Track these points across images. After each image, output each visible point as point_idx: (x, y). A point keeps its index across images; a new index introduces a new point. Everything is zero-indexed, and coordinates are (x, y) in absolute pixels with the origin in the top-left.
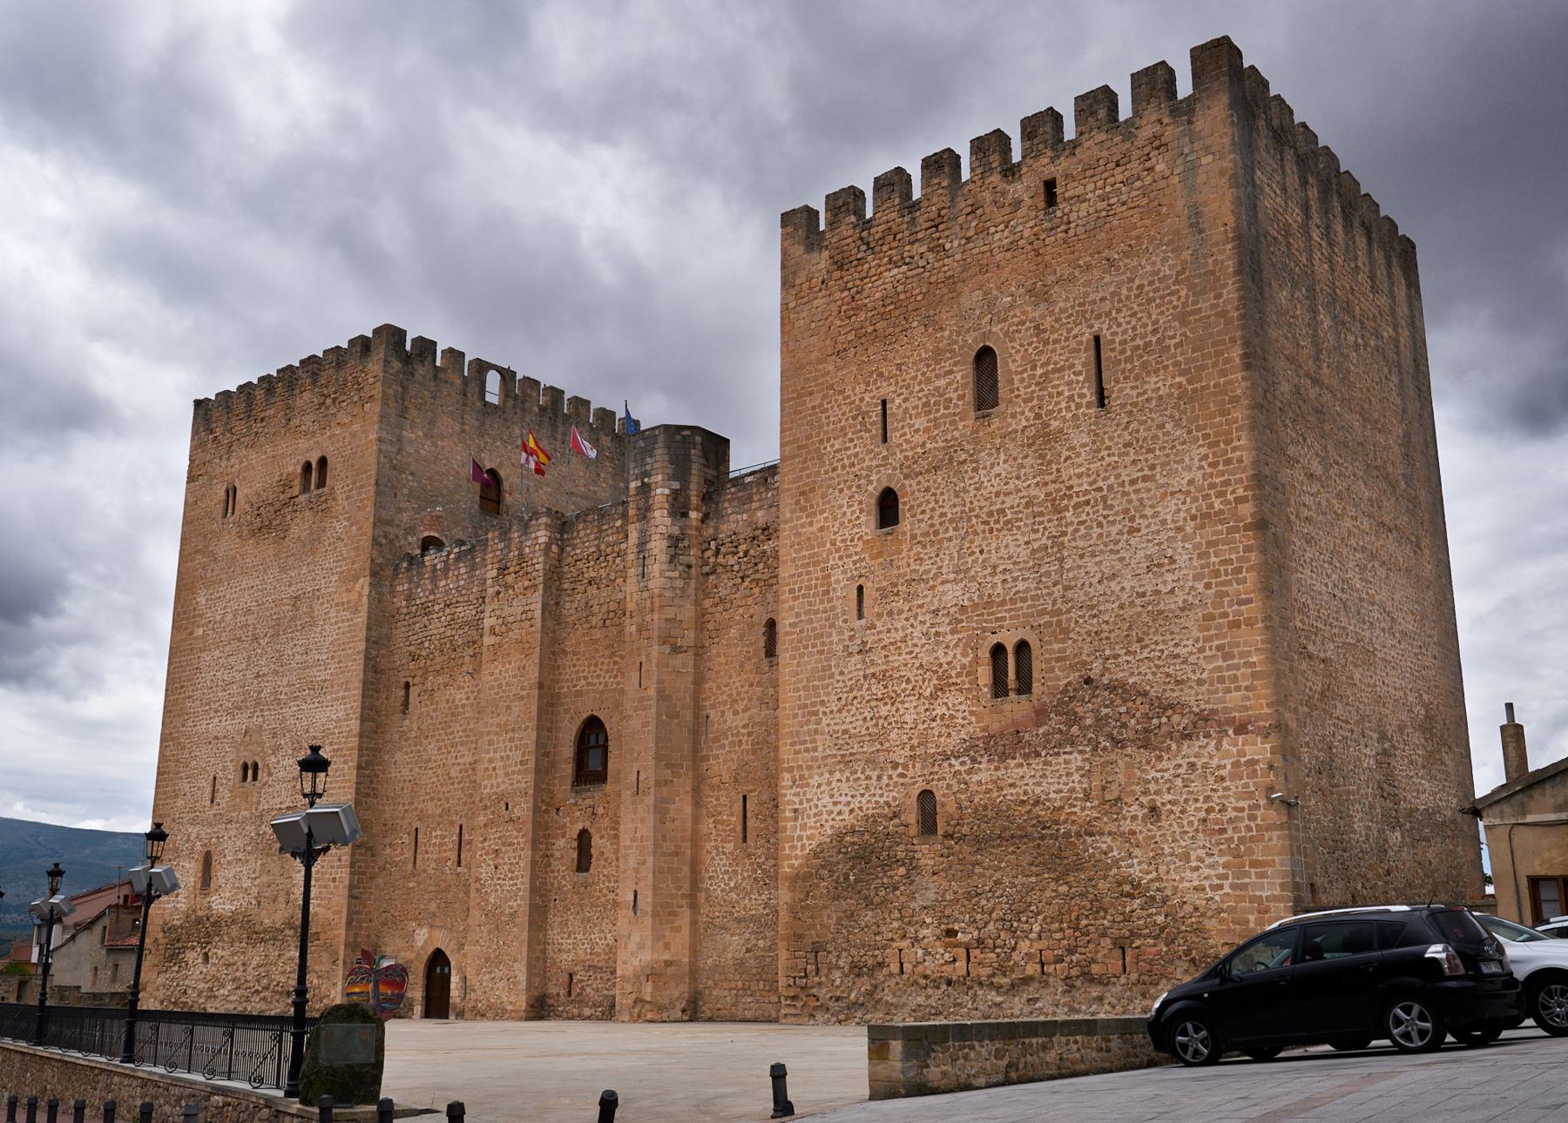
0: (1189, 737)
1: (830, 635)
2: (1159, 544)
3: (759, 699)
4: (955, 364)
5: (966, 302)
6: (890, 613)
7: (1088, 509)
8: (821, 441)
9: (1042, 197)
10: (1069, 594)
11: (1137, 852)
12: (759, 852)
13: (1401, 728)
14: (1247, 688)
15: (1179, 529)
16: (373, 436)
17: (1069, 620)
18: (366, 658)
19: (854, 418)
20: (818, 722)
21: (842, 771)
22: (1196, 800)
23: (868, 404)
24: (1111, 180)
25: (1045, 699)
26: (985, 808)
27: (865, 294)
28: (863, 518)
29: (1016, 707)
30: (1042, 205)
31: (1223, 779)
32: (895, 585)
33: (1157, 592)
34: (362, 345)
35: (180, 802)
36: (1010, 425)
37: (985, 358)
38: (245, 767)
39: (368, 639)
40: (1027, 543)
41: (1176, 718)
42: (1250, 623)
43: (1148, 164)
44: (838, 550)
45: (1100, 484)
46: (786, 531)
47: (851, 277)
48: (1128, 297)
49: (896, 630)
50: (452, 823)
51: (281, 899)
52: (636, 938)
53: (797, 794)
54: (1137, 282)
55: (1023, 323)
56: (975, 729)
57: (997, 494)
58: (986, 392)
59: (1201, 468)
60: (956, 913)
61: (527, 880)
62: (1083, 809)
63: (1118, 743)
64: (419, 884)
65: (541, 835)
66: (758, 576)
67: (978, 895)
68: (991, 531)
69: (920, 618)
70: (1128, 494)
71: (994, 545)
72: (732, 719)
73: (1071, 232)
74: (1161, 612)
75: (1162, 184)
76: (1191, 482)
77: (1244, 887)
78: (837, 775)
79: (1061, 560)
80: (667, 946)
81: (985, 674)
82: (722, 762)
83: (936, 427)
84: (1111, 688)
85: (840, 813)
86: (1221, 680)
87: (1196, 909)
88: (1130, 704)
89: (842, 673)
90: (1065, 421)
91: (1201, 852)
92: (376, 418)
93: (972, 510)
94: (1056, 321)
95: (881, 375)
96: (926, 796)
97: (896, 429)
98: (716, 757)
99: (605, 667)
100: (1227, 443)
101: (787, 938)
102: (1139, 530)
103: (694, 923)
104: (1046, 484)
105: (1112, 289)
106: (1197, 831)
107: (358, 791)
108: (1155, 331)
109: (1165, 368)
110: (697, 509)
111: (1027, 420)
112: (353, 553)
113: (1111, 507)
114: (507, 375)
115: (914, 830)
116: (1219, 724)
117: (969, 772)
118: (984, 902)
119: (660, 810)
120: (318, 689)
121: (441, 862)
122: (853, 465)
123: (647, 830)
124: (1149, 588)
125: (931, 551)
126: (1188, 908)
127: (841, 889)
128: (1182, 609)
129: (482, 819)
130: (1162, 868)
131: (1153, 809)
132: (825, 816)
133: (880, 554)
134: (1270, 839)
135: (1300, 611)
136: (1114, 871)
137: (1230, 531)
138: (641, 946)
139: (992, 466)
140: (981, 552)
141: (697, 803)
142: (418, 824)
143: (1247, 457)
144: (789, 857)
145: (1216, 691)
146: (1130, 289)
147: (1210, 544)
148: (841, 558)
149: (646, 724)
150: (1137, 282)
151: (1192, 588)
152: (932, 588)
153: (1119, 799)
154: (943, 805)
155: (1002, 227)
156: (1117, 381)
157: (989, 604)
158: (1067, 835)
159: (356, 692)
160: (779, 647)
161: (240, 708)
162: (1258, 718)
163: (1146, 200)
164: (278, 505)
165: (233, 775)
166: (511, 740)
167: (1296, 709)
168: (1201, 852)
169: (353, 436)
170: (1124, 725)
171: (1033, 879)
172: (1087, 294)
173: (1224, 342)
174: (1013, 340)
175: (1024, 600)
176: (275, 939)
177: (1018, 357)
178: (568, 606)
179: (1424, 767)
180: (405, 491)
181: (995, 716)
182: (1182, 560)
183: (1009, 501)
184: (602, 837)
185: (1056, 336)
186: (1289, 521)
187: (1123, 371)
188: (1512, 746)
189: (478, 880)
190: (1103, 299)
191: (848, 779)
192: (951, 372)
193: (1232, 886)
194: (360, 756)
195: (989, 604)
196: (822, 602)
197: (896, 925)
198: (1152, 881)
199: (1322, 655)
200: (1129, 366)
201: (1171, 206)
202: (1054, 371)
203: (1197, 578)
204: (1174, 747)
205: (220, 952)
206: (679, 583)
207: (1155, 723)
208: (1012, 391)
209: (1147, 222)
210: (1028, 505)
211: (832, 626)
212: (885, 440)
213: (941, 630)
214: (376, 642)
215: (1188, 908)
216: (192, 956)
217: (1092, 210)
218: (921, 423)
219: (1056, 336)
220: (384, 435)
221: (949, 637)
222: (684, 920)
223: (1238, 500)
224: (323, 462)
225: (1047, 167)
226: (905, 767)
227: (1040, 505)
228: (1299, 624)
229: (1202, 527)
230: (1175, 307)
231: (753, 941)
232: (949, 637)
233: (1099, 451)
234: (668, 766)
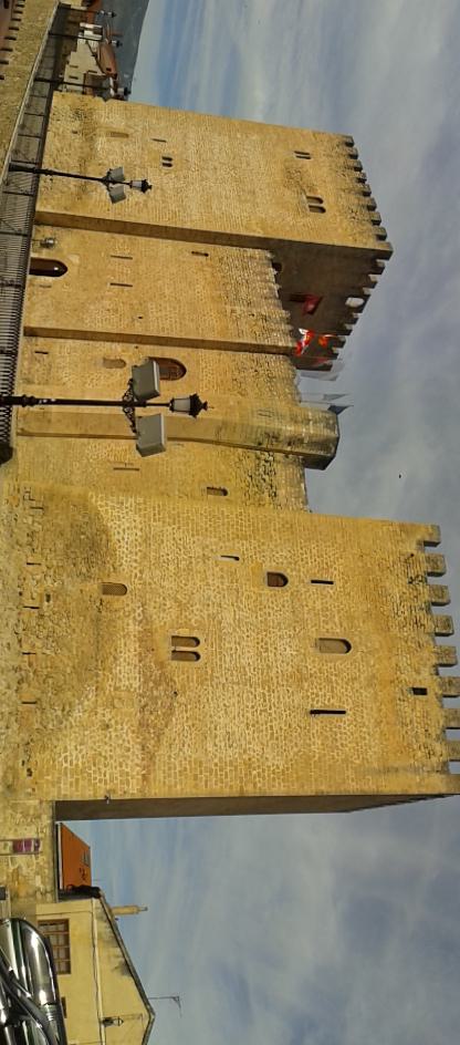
0: (143, 749)
10: (220, 687)
11: (87, 715)
14: (164, 783)
15: (245, 751)
29: (166, 649)
31: (121, 766)
33: (216, 737)
38: (170, 159)
41: (152, 742)
42: (196, 786)
54: (367, 737)
56: (157, 624)
58: (324, 644)
78: (139, 533)
79: (238, 684)
80: (59, 421)
81: (184, 632)
83: (315, 615)
84: (171, 707)
86: (170, 769)
96: (123, 590)
116: (149, 766)
126: (55, 743)
130: (77, 730)
131: (108, 726)
136: (77, 701)
139: (291, 647)
147: (236, 767)
150: (367, 737)
153: (114, 707)
159: (204, 228)
168: (84, 752)
170: (151, 713)
175: (221, 659)
182: (230, 752)
193: (66, 768)
197: (55, 563)
202: (332, 687)
203: (221, 758)
205: (78, 141)
207: (150, 731)
209: (395, 745)
215: (55, 743)
216: (76, 125)
218: (318, 605)
226: (140, 579)
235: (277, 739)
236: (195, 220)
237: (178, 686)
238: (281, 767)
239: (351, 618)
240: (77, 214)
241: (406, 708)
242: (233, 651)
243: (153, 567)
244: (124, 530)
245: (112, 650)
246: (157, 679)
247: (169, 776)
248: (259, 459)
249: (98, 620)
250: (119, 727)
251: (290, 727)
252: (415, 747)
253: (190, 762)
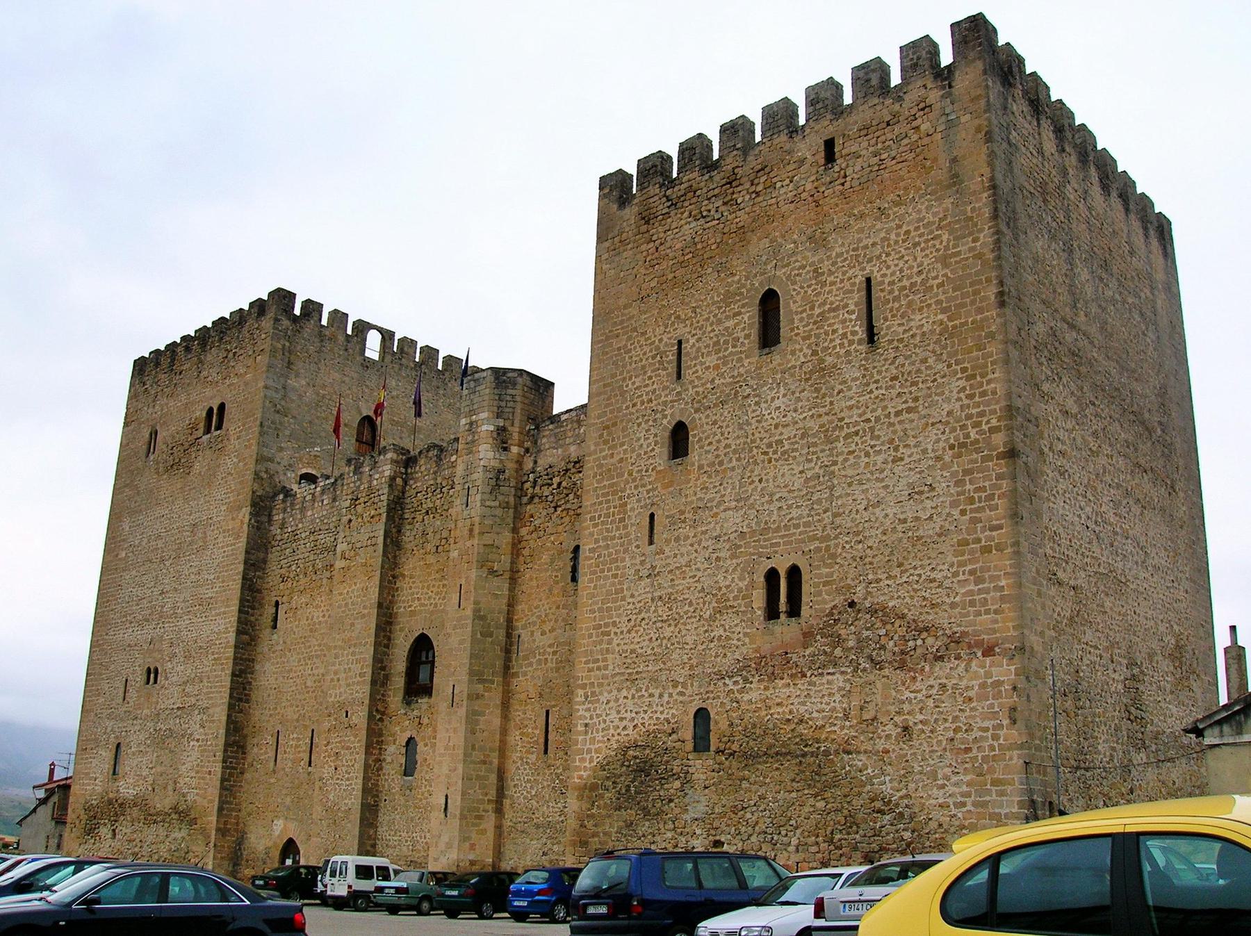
0: (941, 658)
1: (623, 560)
2: (920, 473)
3: (563, 620)
4: (743, 306)
5: (753, 250)
6: (677, 539)
7: (857, 439)
8: (624, 379)
9: (823, 154)
10: (838, 521)
11: (889, 769)
12: (558, 763)
13: (1151, 656)
14: (996, 612)
15: (938, 458)
16: (261, 384)
17: (837, 545)
18: (244, 578)
19: (654, 357)
20: (609, 643)
21: (629, 689)
22: (946, 720)
23: (666, 345)
24: (883, 138)
25: (813, 622)
26: (754, 726)
27: (668, 245)
28: (657, 450)
29: (786, 629)
30: (822, 161)
31: (970, 699)
32: (682, 512)
33: (917, 519)
34: (259, 307)
35: (101, 700)
36: (789, 361)
37: (769, 303)
38: (149, 670)
39: (246, 563)
40: (801, 472)
41: (930, 641)
42: (1000, 548)
43: (914, 124)
44: (634, 480)
45: (868, 416)
46: (590, 465)
47: (657, 231)
48: (896, 242)
49: (682, 555)
50: (305, 727)
51: (170, 788)
52: (445, 838)
53: (588, 710)
54: (905, 228)
55: (803, 267)
56: (747, 650)
57: (776, 427)
58: (769, 335)
59: (959, 399)
60: (723, 827)
61: (360, 781)
62: (842, 728)
63: (877, 664)
64: (278, 780)
65: (375, 739)
66: (568, 506)
67: (744, 808)
68: (770, 462)
69: (703, 544)
70: (892, 425)
71: (772, 474)
72: (535, 637)
73: (847, 185)
74: (919, 538)
75: (926, 141)
76: (949, 413)
77: (984, 804)
78: (624, 693)
79: (832, 488)
80: (472, 847)
81: (759, 598)
82: (527, 680)
83: (725, 364)
84: (873, 611)
85: (625, 728)
86: (972, 603)
87: (940, 825)
88: (889, 627)
89: (632, 596)
90: (839, 356)
91: (948, 771)
92: (265, 369)
93: (753, 441)
94: (834, 264)
95: (678, 317)
96: (702, 716)
97: (689, 367)
98: (525, 674)
99: (435, 590)
100: (982, 376)
101: (574, 844)
102: (902, 459)
103: (499, 827)
104: (820, 416)
105: (883, 235)
106: (945, 749)
107: (231, 696)
108: (920, 272)
109: (929, 306)
111: (805, 356)
112: (239, 487)
113: (879, 437)
114: (387, 336)
115: (690, 746)
116: (970, 646)
117: (741, 691)
118: (748, 815)
119: (472, 719)
120: (205, 604)
121: (296, 762)
122: (651, 401)
123: (459, 739)
124: (910, 515)
125: (716, 480)
126: (933, 825)
127: (626, 799)
128: (940, 535)
129: (326, 725)
130: (912, 786)
131: (906, 729)
132: (612, 731)
133: (671, 484)
134: (1011, 759)
135: (1052, 539)
136: (869, 787)
137: (984, 459)
138: (449, 846)
139: (773, 399)
140: (760, 481)
141: (505, 717)
142: (279, 727)
143: (1000, 389)
144: (578, 769)
145: (967, 615)
146: (898, 235)
147: (966, 472)
148: (636, 487)
149: (461, 642)
150: (905, 228)
151: (949, 514)
152: (716, 515)
153: (874, 719)
154: (717, 723)
155: (787, 181)
156: (886, 319)
157: (767, 529)
158: (827, 753)
159: (234, 608)
160: (581, 570)
161: (147, 620)
162: (1006, 640)
163: (913, 155)
164: (186, 446)
165: (141, 678)
166: (353, 654)
167: (1042, 633)
168: (948, 771)
169: (243, 384)
170: (883, 647)
171: (794, 795)
172: (860, 240)
173: (980, 282)
174: (794, 283)
175: (797, 526)
176: (164, 821)
177: (798, 298)
178: (408, 534)
179: (1172, 692)
180: (287, 433)
181: (766, 637)
182: (941, 487)
183: (787, 432)
184: (426, 745)
185: (832, 278)
186: (1042, 453)
187: (891, 310)
188: (1234, 667)
189: (321, 779)
190: (874, 244)
191: (633, 697)
192: (739, 313)
193: (974, 804)
194: (235, 664)
195: (767, 529)
196: (618, 529)
197: (669, 835)
198: (901, 798)
199: (1072, 583)
200: (896, 305)
201: (935, 160)
202: (831, 310)
203: (954, 504)
204: (927, 668)
205: (125, 829)
207: (911, 645)
208: (792, 330)
209: (914, 175)
210: (803, 436)
211: (626, 551)
212: (679, 376)
213: (722, 555)
214: (253, 565)
215: (933, 825)
216: (105, 831)
217: (865, 165)
218: (711, 360)
219: (832, 278)
220: (270, 383)
221: (729, 562)
222: (489, 822)
223: (993, 430)
224: (222, 407)
225: (827, 128)
226: (684, 685)
227: (814, 435)
228: (1049, 552)
229: (959, 456)
230: (938, 250)
231: (549, 846)
232: (729, 562)
233: (868, 384)
234: (481, 681)
235: (916, 399)
236: (221, 627)
237: (839, 600)
238: (962, 383)
239: (728, 298)
240: (214, 825)
241: (854, 170)
242: (783, 504)
243: (669, 664)
244: (621, 719)
245: (788, 728)
246: (829, 648)
247: (984, 602)
248: (532, 498)
249: (745, 755)
250: (906, 707)
251: (894, 378)
252: (915, 137)
253: (961, 564)
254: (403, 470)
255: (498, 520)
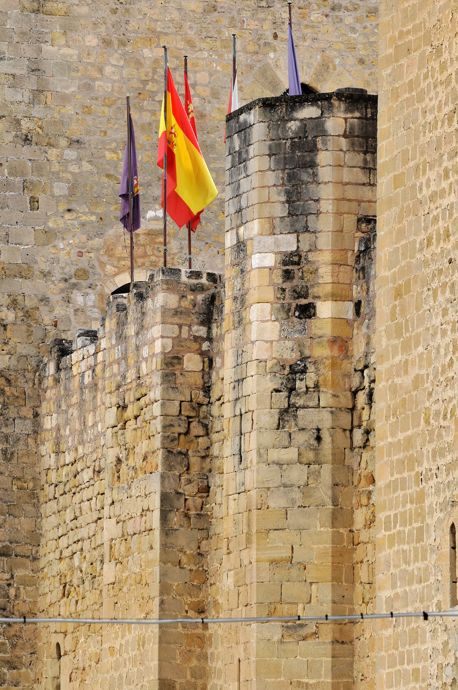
110: (336, 297)
180: (60, 189)
206: (298, 474)
254: (202, 331)
255: (296, 495)
